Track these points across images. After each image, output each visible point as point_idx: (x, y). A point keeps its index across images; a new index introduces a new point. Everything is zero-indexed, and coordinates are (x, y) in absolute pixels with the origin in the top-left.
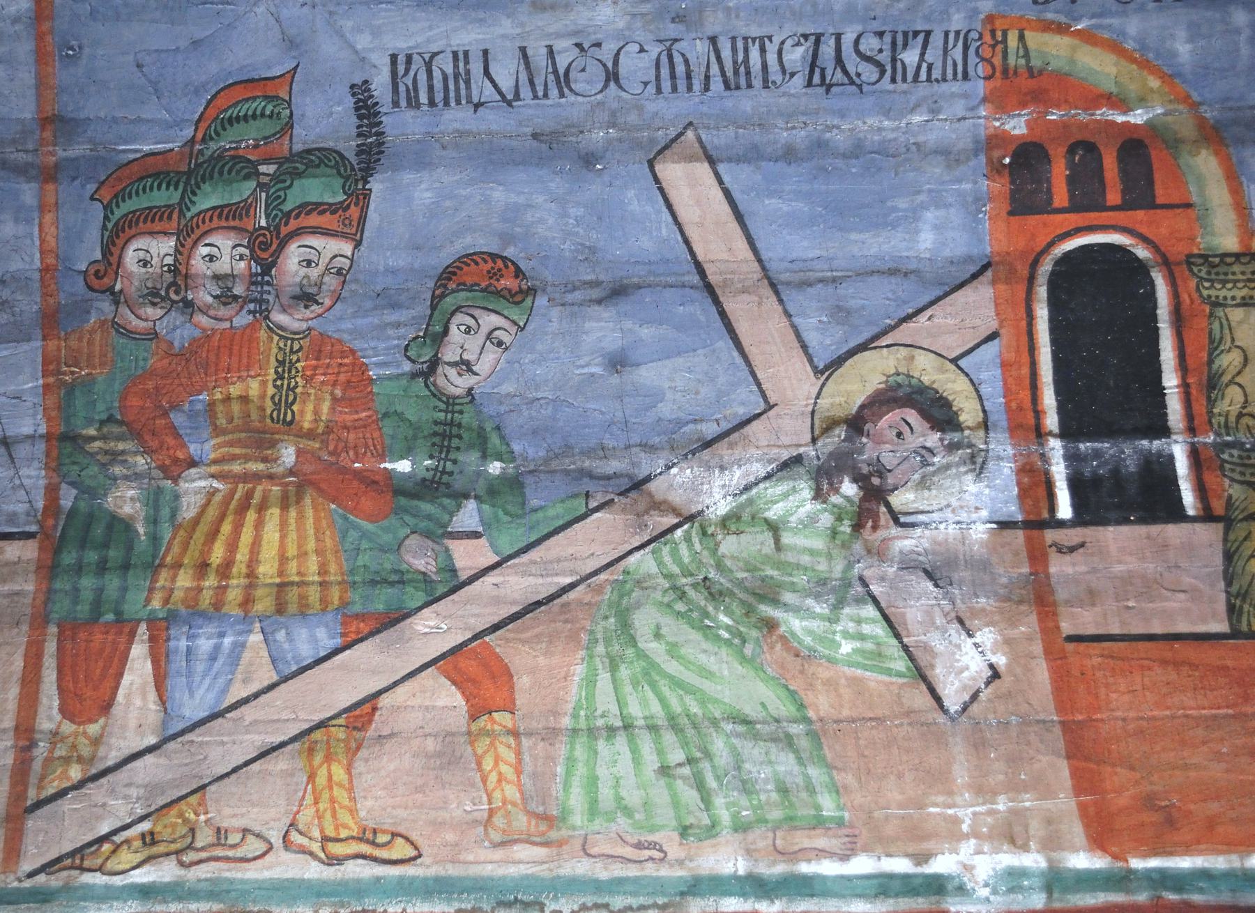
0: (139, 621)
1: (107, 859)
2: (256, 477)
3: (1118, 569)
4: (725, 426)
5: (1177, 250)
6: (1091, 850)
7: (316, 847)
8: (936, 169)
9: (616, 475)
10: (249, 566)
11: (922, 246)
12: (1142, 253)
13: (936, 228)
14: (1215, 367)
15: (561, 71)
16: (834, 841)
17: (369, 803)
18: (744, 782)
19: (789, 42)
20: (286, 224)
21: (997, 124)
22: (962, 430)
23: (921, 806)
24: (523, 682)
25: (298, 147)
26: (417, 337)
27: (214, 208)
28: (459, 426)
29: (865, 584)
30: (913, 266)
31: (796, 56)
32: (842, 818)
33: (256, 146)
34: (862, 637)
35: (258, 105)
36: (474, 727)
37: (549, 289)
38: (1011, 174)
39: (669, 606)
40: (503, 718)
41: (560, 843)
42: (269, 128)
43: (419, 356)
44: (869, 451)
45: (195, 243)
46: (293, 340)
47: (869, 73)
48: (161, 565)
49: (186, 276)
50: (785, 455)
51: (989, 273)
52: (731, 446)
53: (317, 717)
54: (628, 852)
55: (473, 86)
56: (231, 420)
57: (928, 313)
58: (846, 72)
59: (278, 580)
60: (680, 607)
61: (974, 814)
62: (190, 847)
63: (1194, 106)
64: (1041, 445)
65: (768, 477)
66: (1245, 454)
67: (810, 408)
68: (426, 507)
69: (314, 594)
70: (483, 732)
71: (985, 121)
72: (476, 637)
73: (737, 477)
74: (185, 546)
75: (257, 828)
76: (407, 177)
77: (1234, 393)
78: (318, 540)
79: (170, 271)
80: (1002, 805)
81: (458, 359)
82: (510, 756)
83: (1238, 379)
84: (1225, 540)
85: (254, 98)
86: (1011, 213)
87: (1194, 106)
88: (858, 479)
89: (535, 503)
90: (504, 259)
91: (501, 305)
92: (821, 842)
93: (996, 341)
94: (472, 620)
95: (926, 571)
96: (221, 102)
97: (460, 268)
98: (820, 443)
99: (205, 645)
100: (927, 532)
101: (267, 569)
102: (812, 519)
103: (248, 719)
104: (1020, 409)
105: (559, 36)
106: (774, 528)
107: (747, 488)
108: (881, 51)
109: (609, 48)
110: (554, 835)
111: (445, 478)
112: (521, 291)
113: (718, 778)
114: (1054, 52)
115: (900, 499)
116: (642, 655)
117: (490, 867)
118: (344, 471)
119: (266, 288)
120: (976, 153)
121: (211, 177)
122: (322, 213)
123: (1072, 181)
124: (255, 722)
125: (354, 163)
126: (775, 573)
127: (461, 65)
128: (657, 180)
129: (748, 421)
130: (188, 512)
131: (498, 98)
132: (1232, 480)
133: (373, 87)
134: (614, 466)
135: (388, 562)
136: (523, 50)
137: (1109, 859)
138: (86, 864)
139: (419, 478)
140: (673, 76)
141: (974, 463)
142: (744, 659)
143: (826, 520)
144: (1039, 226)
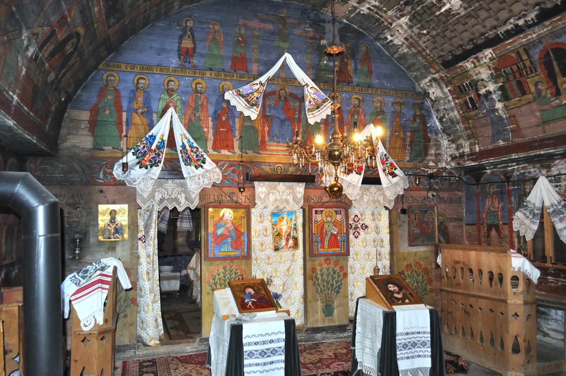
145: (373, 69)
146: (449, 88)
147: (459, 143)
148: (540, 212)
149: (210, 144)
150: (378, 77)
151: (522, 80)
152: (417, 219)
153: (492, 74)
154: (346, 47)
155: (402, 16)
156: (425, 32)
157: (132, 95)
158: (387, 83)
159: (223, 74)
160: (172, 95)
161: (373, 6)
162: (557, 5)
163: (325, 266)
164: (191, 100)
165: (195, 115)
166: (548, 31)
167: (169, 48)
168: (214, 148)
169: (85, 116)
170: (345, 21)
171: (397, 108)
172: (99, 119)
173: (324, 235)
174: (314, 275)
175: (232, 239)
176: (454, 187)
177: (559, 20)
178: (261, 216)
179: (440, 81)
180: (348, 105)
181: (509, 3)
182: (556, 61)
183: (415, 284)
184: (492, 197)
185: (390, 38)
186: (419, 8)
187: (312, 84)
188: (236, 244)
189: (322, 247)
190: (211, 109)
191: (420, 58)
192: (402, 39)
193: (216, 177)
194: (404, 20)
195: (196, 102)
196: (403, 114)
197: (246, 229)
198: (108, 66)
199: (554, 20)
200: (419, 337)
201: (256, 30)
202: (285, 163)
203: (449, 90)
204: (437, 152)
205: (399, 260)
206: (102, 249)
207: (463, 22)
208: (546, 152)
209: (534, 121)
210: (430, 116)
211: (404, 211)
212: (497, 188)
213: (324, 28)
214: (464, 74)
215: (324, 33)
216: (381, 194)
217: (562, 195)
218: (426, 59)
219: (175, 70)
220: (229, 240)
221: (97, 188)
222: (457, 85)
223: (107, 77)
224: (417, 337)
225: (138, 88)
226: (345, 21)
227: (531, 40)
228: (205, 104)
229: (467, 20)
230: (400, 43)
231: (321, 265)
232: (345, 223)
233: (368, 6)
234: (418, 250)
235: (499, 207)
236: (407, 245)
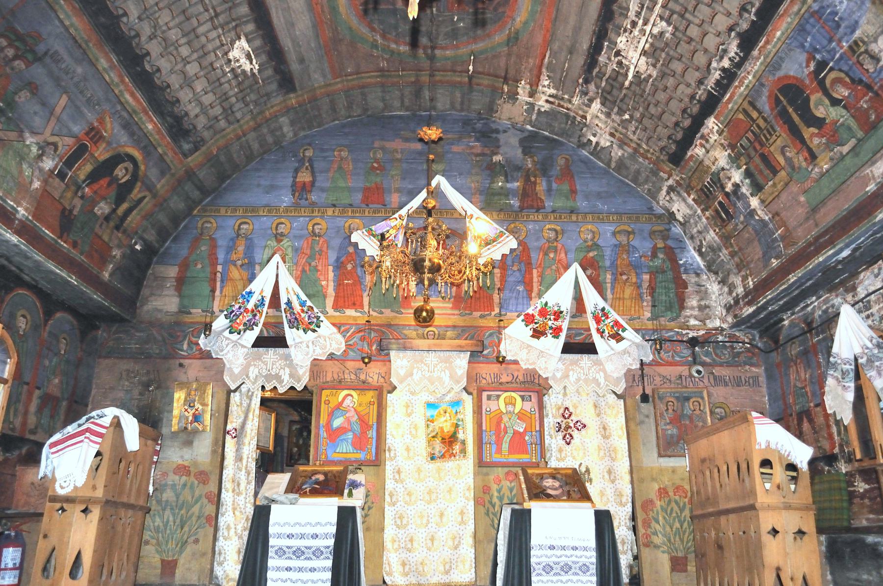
145: (578, 187)
146: (692, 197)
147: (730, 282)
148: (853, 367)
149: (330, 302)
150: (587, 197)
151: (765, 151)
152: (670, 411)
153: (729, 154)
154: (534, 161)
155: (591, 101)
156: (627, 117)
157: (231, 244)
158: (603, 205)
159: (350, 210)
160: (282, 241)
161: (550, 96)
162: (753, 21)
163: (506, 484)
164: (305, 245)
165: (310, 265)
166: (762, 64)
167: (279, 184)
168: (336, 307)
169: (172, 272)
170: (529, 127)
171: (623, 239)
172: (189, 275)
173: (503, 433)
174: (487, 498)
175: (354, 434)
176: (742, 358)
177: (767, 42)
178: (407, 406)
179: (678, 189)
180: (538, 239)
181: (697, 39)
182: (791, 105)
183: (677, 525)
184: (796, 364)
185: (594, 140)
186: (603, 84)
187: (477, 212)
188: (360, 443)
189: (499, 451)
190: (332, 256)
191: (641, 160)
192: (608, 137)
193: (335, 346)
194: (596, 106)
195: (312, 248)
196: (634, 247)
197: (375, 420)
198: (205, 211)
199: (761, 44)
200: (576, 557)
201: (397, 152)
202: (440, 326)
203: (694, 200)
204: (703, 303)
205: (642, 480)
206: (176, 444)
207: (661, 87)
208: (824, 256)
209: (801, 211)
210: (683, 249)
211: (645, 398)
212: (800, 346)
213: (498, 140)
214: (701, 167)
215: (498, 147)
216: (446, 367)
217: (878, 329)
218: (647, 158)
219: (287, 210)
220: (350, 435)
221: (177, 362)
222: (699, 187)
223: (203, 224)
224: (571, 556)
225: (238, 235)
226: (529, 127)
227: (751, 86)
228: (324, 249)
229: (664, 81)
230: (608, 144)
231: (498, 481)
232: (537, 415)
233: (544, 98)
234: (677, 465)
235: (805, 380)
236: (656, 455)
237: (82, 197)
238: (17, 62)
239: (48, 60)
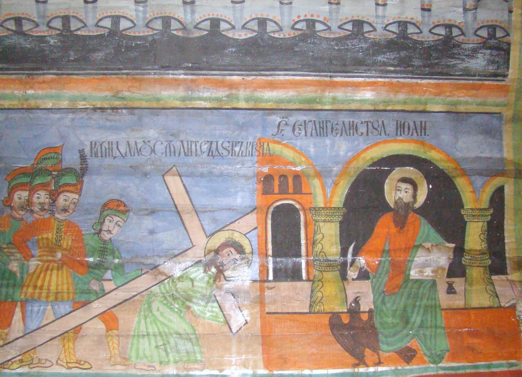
0: (18, 301)
1: (10, 366)
2: (50, 261)
3: (283, 294)
4: (181, 251)
5: (307, 206)
6: (265, 369)
7: (65, 364)
8: (243, 181)
9: (150, 264)
10: (48, 287)
11: (238, 202)
12: (298, 206)
13: (242, 197)
14: (315, 238)
15: (139, 148)
16: (200, 366)
17: (79, 353)
18: (178, 350)
19: (203, 143)
20: (60, 189)
21: (260, 169)
22: (246, 254)
23: (222, 357)
24: (121, 322)
25: (63, 167)
26: (96, 223)
27: (39, 184)
28: (107, 248)
29: (215, 296)
30: (235, 208)
31: (205, 147)
32: (202, 360)
33: (52, 166)
34: (212, 312)
35: (53, 155)
36: (107, 334)
37: (134, 210)
38: (263, 183)
39: (162, 301)
40: (115, 332)
41: (128, 365)
42: (56, 161)
43: (97, 228)
44: (220, 259)
45: (34, 193)
46: (61, 222)
47: (225, 153)
48: (24, 286)
49: (31, 203)
50: (197, 260)
51: (256, 211)
52: (182, 257)
53: (66, 330)
54: (146, 368)
55: (114, 152)
56: (43, 245)
57: (238, 221)
58: (219, 153)
59: (56, 291)
60: (165, 302)
61: (236, 360)
62: (32, 363)
63: (314, 166)
64: (267, 259)
65: (192, 266)
66: (320, 263)
67: (205, 247)
68: (97, 271)
69: (65, 296)
70: (109, 335)
71: (257, 168)
72: (109, 309)
73: (183, 266)
74: (31, 280)
75: (50, 359)
76: (94, 177)
77: (319, 246)
78: (67, 280)
79: (27, 201)
80: (243, 357)
81: (107, 229)
82: (117, 342)
83: (321, 242)
84: (312, 287)
85: (51, 153)
86: (263, 194)
87: (314, 166)
88: (217, 267)
89: (127, 271)
90: (121, 201)
91: (121, 215)
92: (196, 366)
93: (257, 230)
94: (108, 305)
95: (232, 293)
96: (41, 154)
97: (110, 202)
98: (207, 257)
99: (36, 309)
100: (233, 283)
101: (53, 288)
102: (203, 278)
103: (47, 330)
104: (262, 249)
105: (138, 138)
106: (192, 280)
107: (186, 269)
108: (229, 147)
109: (153, 142)
110: (127, 363)
111: (103, 263)
112: (125, 211)
113: (171, 349)
114: (277, 149)
115: (227, 273)
116: (154, 315)
117: (110, 371)
118: (74, 260)
119: (54, 207)
120: (254, 177)
121: (39, 175)
122: (70, 186)
123: (280, 185)
124: (49, 331)
125: (79, 172)
126: (191, 293)
127: (110, 145)
128: (164, 181)
129: (187, 250)
130: (31, 271)
131: (121, 155)
132: (316, 270)
133: (85, 151)
134: (150, 261)
135: (86, 287)
136: (128, 142)
137: (268, 371)
138: (5, 367)
139: (95, 263)
140: (170, 151)
141: (248, 263)
142: (181, 317)
143: (207, 279)
144: (270, 198)
237: (363, 275)
238: (61, 200)
239: (93, 162)
